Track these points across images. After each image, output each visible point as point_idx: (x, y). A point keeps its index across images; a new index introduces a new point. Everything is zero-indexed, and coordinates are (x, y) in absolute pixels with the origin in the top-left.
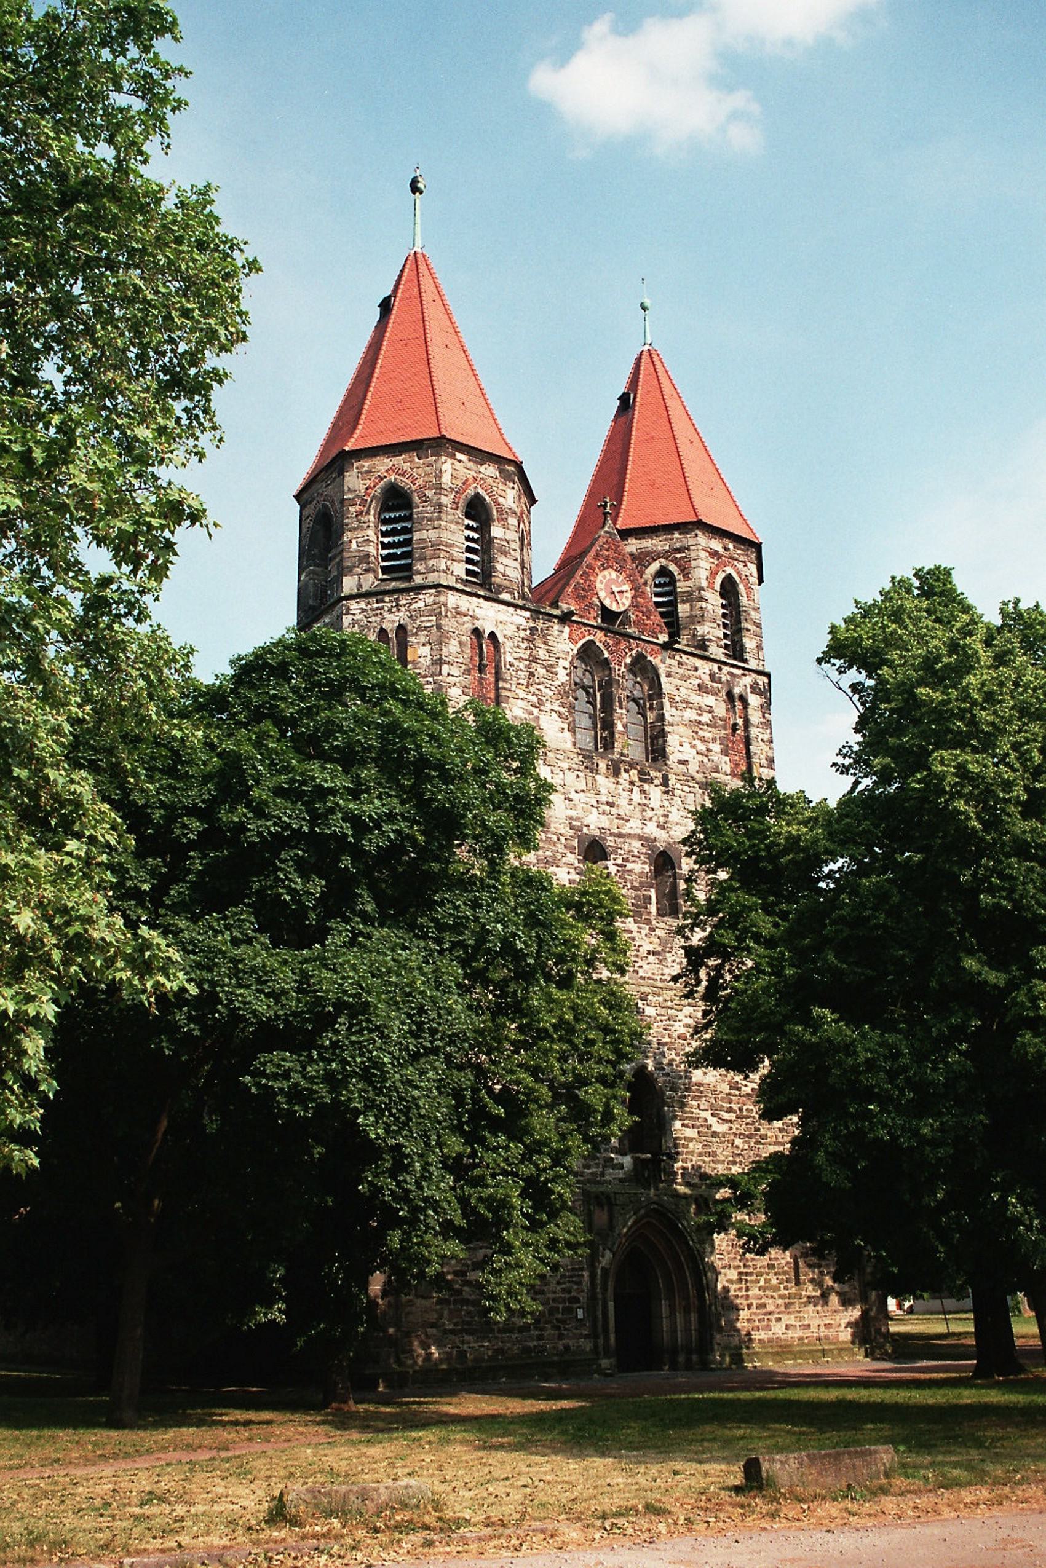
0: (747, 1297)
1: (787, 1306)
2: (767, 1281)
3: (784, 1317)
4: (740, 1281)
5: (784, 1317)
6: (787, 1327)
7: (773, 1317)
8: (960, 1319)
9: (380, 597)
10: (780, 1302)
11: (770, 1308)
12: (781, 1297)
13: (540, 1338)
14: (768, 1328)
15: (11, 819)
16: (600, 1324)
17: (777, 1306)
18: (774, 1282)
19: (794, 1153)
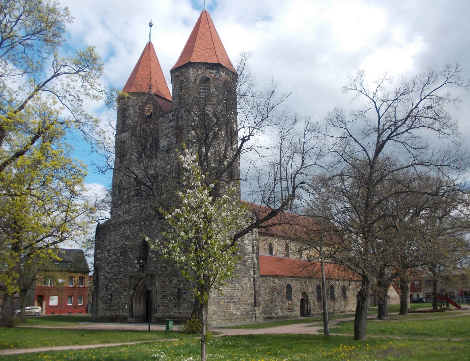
0: (164, 303)
1: (175, 306)
2: (170, 298)
3: (174, 309)
4: (162, 298)
5: (174, 309)
6: (175, 312)
7: (171, 309)
8: (418, 320)
9: (255, 252)
10: (173, 304)
11: (170, 306)
12: (173, 303)
13: (119, 312)
14: (169, 312)
15: (385, 348)
16: (458, 315)
17: (172, 306)
18: (172, 298)
19: (117, 166)
